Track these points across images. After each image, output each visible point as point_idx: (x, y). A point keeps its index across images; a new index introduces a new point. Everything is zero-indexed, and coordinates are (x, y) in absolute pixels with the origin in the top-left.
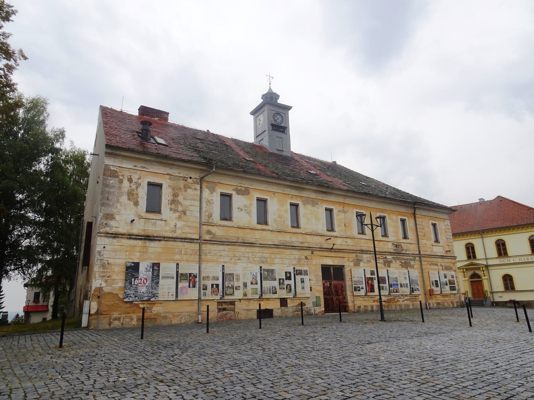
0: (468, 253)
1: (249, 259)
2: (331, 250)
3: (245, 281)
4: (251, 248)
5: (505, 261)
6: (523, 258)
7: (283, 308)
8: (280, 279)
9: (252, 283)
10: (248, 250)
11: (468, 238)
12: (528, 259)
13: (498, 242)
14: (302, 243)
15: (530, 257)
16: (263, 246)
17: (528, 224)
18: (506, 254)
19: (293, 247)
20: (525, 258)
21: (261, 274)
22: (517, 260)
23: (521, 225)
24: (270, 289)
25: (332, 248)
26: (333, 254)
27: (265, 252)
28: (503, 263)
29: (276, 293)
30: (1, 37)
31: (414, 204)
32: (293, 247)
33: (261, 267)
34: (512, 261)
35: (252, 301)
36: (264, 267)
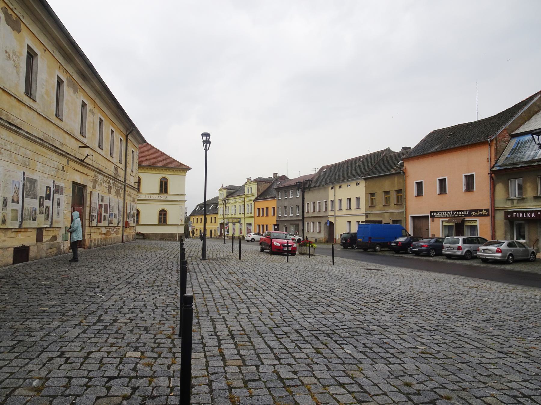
0: (161, 187)
1: (11, 155)
2: (82, 162)
3: (5, 196)
4: (15, 136)
5: (163, 197)
6: (152, 196)
7: (39, 244)
8: (41, 197)
9: (13, 201)
10: (11, 139)
11: (165, 173)
12: (155, 197)
13: (162, 180)
14: (62, 144)
15: (157, 196)
16: (29, 137)
17: (163, 167)
18: (166, 191)
19: (56, 150)
20: (154, 196)
21: (24, 184)
22: (147, 197)
23: (168, 167)
24: (30, 211)
25: (82, 161)
26: (81, 169)
27: (29, 148)
28: (163, 199)
29: (34, 220)
30: (2, 314)
31: (130, 129)
32: (56, 150)
33: (24, 173)
34: (142, 198)
35: (9, 233)
36: (28, 175)
